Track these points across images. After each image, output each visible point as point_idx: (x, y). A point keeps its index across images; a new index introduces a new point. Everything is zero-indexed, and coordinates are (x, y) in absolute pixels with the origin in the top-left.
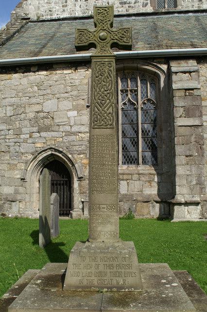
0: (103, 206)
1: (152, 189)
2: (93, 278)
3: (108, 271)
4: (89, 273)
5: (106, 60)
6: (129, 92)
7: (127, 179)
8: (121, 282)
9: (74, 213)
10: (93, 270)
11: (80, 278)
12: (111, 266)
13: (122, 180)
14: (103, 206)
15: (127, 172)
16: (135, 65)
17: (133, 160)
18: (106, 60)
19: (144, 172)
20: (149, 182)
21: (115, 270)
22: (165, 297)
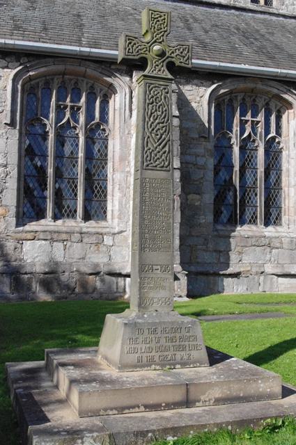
0: (157, 267)
1: (101, 255)
2: (153, 354)
3: (170, 344)
4: (149, 348)
5: (161, 83)
6: (68, 109)
7: (64, 240)
8: (185, 357)
9: (129, 271)
10: (153, 345)
11: (137, 355)
12: (172, 340)
13: (56, 241)
14: (157, 267)
15: (64, 229)
16: (82, 69)
17: (70, 211)
18: (161, 83)
19: (89, 230)
20: (97, 244)
21: (177, 343)
22: (242, 369)
